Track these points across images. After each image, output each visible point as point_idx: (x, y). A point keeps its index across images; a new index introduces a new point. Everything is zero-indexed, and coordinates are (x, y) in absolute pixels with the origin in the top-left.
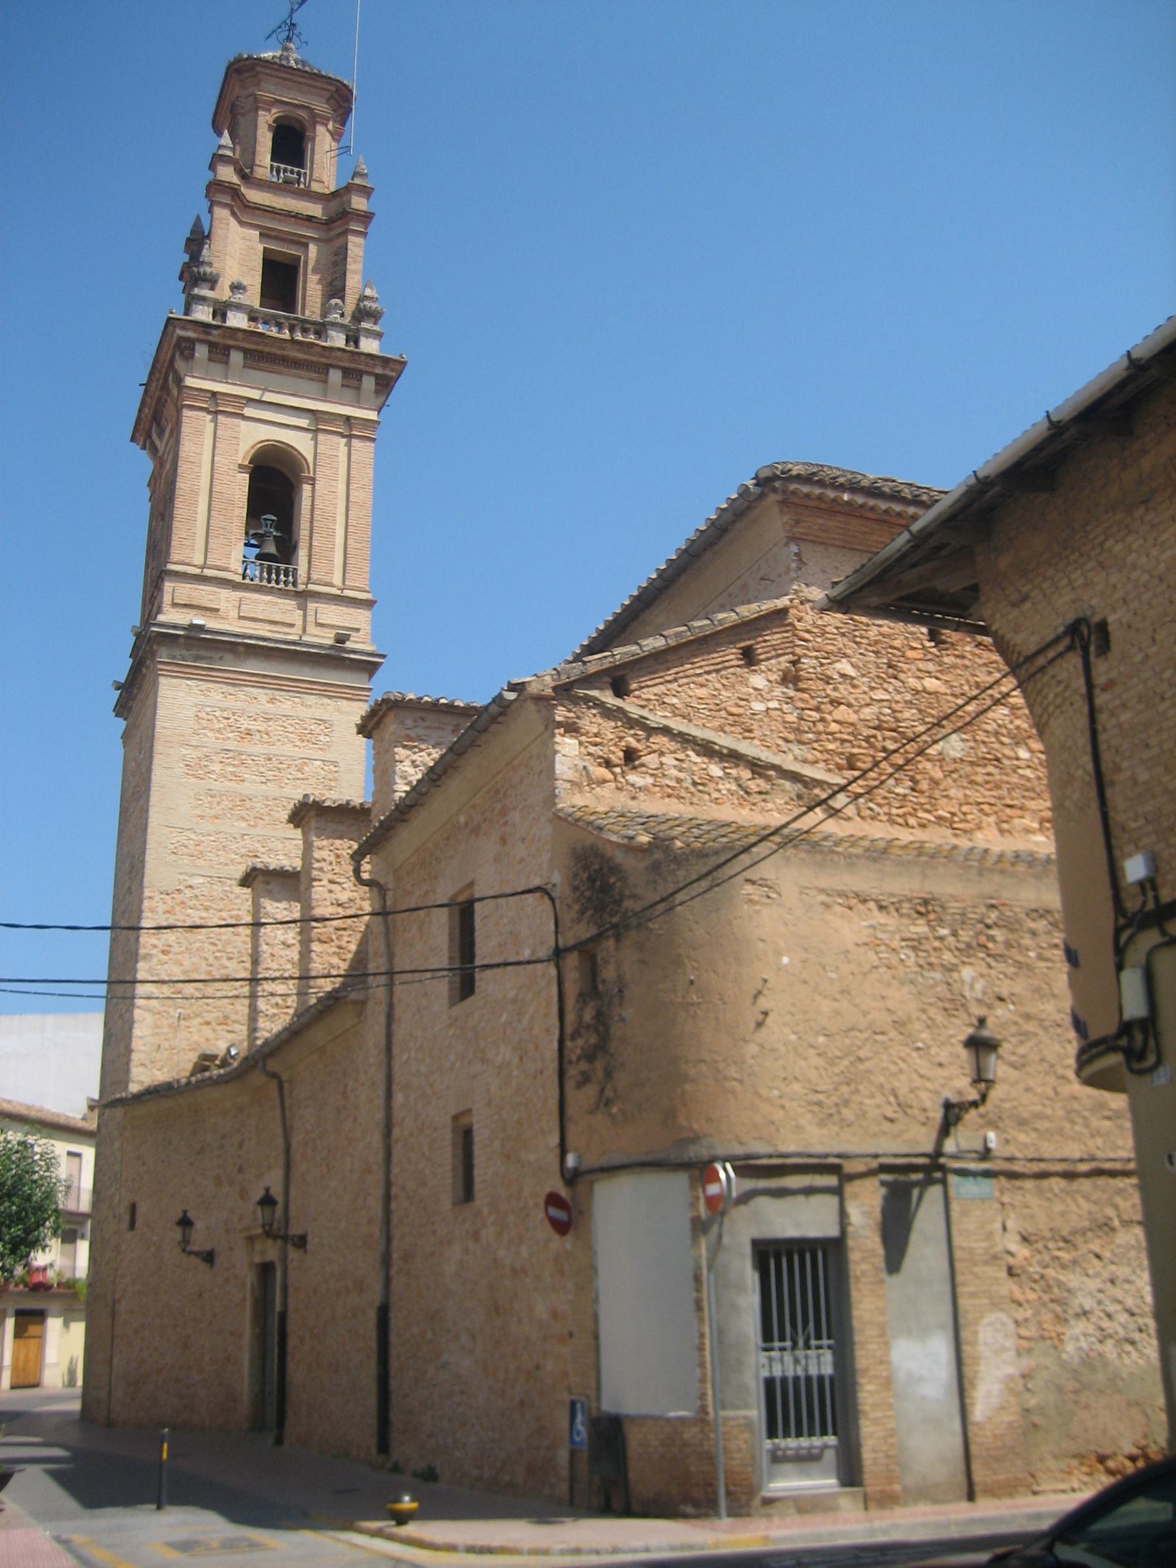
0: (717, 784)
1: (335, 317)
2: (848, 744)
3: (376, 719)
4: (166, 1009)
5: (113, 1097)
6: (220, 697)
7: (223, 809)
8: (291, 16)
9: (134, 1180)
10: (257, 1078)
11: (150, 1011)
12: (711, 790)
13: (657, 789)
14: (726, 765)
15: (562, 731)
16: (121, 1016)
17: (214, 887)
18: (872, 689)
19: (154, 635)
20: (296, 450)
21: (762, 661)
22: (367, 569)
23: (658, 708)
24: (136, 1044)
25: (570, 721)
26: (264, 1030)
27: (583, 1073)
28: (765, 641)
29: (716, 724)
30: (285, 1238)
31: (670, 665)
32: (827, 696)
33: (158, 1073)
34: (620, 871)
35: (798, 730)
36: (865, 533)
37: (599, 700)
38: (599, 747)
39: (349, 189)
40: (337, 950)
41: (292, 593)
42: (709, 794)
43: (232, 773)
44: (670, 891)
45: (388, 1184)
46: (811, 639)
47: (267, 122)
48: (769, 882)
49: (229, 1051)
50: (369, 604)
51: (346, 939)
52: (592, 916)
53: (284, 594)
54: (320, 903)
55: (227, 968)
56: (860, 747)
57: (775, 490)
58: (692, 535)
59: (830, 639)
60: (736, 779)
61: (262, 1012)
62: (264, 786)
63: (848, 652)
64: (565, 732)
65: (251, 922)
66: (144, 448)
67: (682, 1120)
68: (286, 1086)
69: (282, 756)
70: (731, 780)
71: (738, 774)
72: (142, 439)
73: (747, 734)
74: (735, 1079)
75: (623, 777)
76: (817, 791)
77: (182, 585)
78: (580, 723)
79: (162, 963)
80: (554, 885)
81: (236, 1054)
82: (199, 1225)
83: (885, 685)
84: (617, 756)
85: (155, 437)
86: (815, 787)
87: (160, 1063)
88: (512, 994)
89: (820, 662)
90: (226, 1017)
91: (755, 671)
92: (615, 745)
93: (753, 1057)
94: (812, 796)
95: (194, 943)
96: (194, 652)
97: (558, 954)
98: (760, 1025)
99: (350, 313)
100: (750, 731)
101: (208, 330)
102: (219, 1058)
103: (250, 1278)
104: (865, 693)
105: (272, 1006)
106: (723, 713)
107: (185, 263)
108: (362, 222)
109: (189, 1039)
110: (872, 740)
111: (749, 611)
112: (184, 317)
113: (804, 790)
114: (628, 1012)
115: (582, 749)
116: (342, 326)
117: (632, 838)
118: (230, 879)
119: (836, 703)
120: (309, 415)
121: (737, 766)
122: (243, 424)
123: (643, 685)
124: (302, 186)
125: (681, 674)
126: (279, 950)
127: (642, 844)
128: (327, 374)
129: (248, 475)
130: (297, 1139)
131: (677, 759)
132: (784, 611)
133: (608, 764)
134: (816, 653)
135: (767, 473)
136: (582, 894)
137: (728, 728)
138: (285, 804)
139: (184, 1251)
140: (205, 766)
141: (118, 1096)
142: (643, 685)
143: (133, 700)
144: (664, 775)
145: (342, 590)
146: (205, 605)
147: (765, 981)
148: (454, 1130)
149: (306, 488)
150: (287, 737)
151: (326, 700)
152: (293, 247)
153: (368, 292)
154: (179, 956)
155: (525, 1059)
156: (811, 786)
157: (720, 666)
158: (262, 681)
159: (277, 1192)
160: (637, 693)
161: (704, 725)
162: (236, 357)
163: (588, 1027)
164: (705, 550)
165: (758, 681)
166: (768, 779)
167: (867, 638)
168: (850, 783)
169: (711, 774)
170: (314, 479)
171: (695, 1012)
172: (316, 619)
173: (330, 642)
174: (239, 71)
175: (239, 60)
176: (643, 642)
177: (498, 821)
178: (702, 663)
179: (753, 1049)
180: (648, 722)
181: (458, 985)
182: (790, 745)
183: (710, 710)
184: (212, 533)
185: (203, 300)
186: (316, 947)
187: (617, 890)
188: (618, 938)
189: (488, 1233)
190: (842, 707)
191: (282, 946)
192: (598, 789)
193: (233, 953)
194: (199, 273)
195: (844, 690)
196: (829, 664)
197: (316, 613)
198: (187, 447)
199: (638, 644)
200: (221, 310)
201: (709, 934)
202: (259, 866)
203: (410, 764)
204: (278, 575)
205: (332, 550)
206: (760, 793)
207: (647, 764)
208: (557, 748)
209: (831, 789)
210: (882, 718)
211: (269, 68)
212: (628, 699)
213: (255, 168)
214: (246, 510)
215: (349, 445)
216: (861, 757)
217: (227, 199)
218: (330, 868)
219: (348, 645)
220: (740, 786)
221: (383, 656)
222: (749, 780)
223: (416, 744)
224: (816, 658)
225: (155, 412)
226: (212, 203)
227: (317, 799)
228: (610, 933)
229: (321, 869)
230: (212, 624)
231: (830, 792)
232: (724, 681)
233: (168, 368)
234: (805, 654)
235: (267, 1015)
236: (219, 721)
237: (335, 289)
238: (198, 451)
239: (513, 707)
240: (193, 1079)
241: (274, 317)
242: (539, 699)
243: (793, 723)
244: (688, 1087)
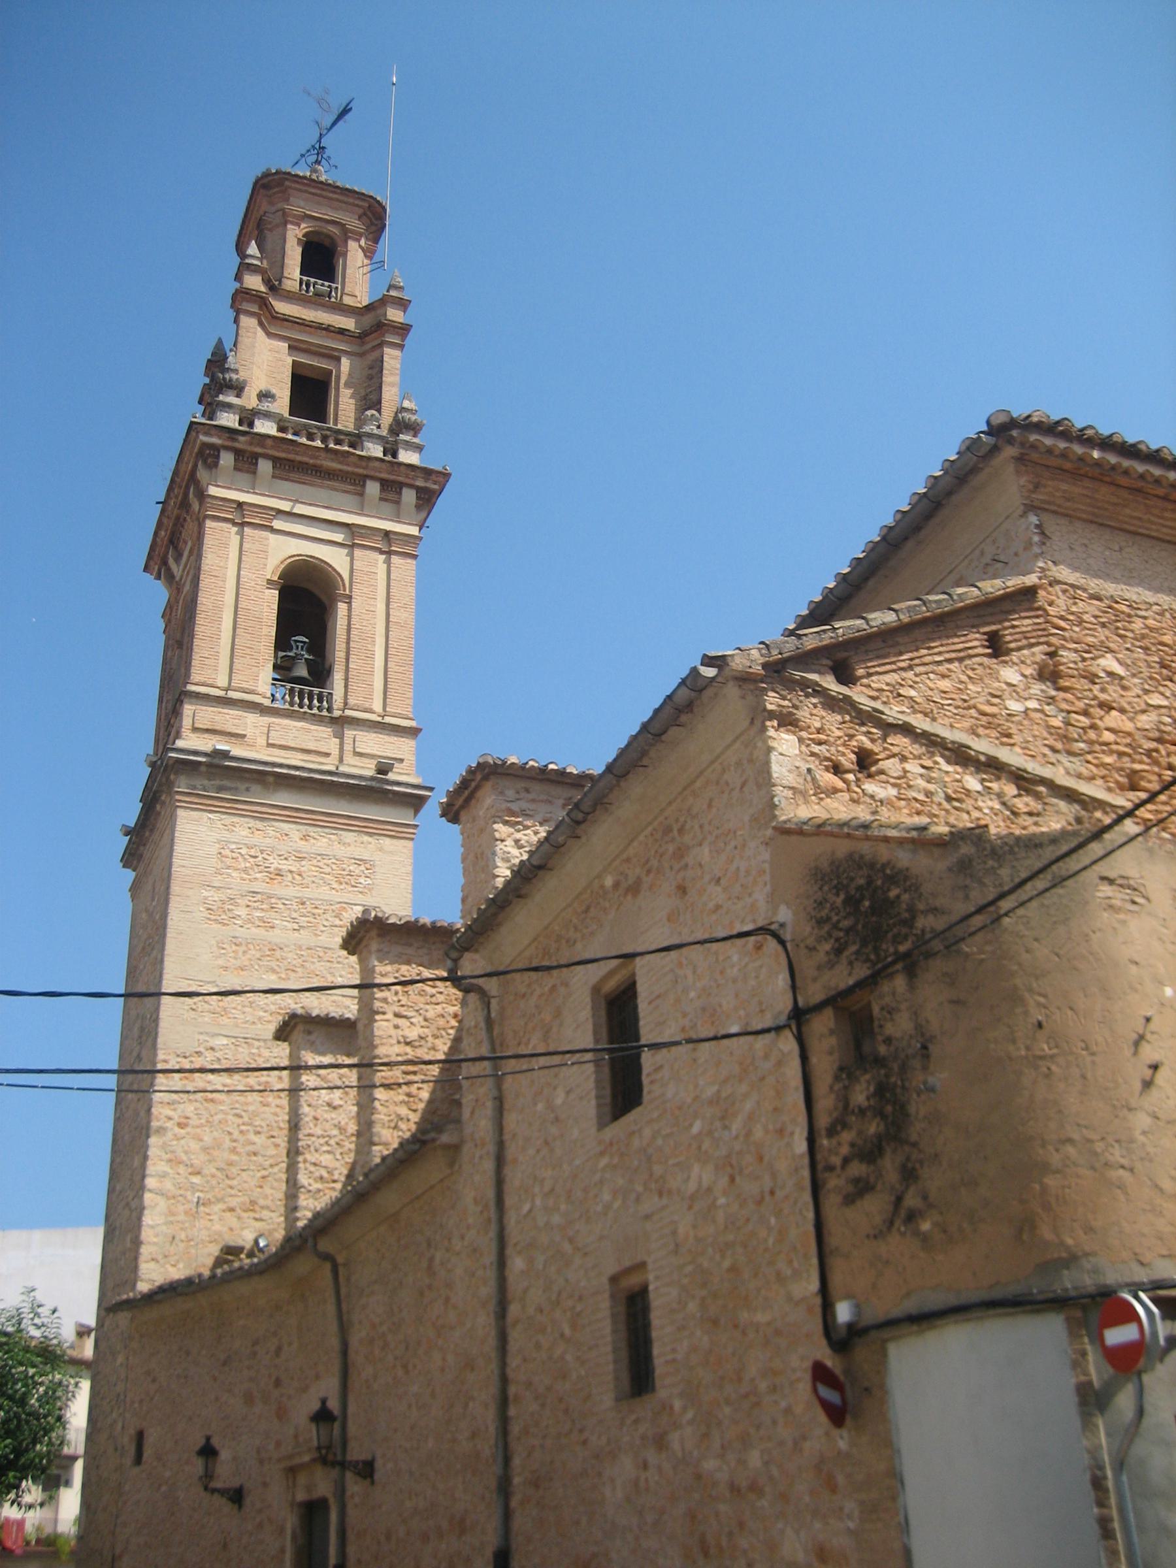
0: (976, 800)
1: (370, 428)
2: (1126, 759)
3: (467, 793)
4: (181, 1192)
5: (118, 1298)
6: (246, 832)
7: (250, 960)
8: (319, 141)
9: (141, 1401)
10: (303, 1265)
11: (163, 1194)
12: (970, 808)
13: (903, 803)
14: (985, 776)
15: (775, 723)
16: (128, 1204)
17: (240, 1049)
18: (1147, 692)
19: (171, 762)
20: (331, 566)
21: (1012, 650)
22: (411, 695)
23: (892, 701)
24: (146, 1234)
25: (785, 711)
26: (306, 1208)
27: (856, 1181)
28: (1014, 627)
29: (967, 724)
30: (343, 1465)
31: (902, 648)
32: (1095, 698)
33: (171, 1269)
34: (906, 878)
35: (1065, 738)
36: (1115, 504)
37: (820, 686)
39: (384, 301)
40: (406, 1099)
41: (327, 720)
42: (968, 813)
43: (261, 919)
44: (991, 897)
45: (504, 1380)
46: (1068, 627)
47: (296, 236)
48: (1132, 882)
49: (256, 1242)
50: (413, 732)
53: (318, 720)
54: (385, 1041)
55: (254, 1144)
56: (1141, 762)
57: (1011, 441)
58: (889, 521)
59: (1089, 629)
60: (1000, 796)
61: (303, 1187)
62: (296, 934)
63: (1111, 645)
64: (779, 725)
65: (358, 982)
66: (158, 577)
67: (1046, 1232)
68: (341, 1271)
69: (317, 899)
70: (993, 797)
71: (1001, 788)
72: (156, 567)
73: (1005, 740)
74: (1123, 1167)
75: (859, 787)
76: (1098, 814)
77: (204, 708)
78: (799, 714)
79: (178, 1138)
80: (782, 925)
81: (267, 1246)
82: (224, 1455)
83: (1161, 689)
84: (848, 760)
85: (171, 561)
86: (1095, 809)
87: (176, 1257)
88: (710, 1091)
89: (1081, 656)
90: (253, 1203)
91: (1006, 662)
92: (844, 745)
93: (1144, 1133)
94: (1093, 821)
95: (216, 1114)
96: (218, 782)
97: (799, 1016)
98: (1148, 1084)
99: (387, 426)
100: (1009, 736)
101: (236, 437)
102: (245, 1251)
103: (291, 1521)
104: (1139, 696)
105: (315, 1180)
106: (973, 711)
107: (205, 384)
108: (398, 334)
109: (208, 1229)
110: (1154, 754)
111: (992, 587)
112: (208, 422)
113: (1083, 813)
114: (939, 1077)
115: (803, 748)
116: (380, 437)
117: (924, 828)
118: (258, 1040)
119: (1107, 707)
120: (344, 530)
121: (998, 778)
122: (272, 537)
123: (872, 670)
124: (333, 300)
125: (917, 661)
126: (325, 1114)
127: (941, 835)
128: (364, 486)
129: (277, 592)
130: (356, 1338)
131: (923, 767)
132: (1030, 592)
133: (837, 769)
134: (1075, 645)
135: (1002, 419)
136: (836, 926)
137: (981, 731)
138: (321, 954)
139: (206, 1489)
140: (229, 910)
141: (125, 1297)
142: (872, 670)
143: (144, 845)
144: (910, 786)
145: (383, 717)
146: (229, 730)
147: (1148, 1020)
148: (613, 1296)
149: (342, 607)
150: (323, 879)
151: (366, 838)
152: (325, 361)
153: (406, 404)
154: (198, 1130)
155: (738, 1179)
156: (1090, 807)
157: (962, 654)
158: (294, 816)
159: (334, 1405)
160: (865, 681)
161: (952, 726)
162: (265, 466)
163: (862, 1112)
164: (906, 539)
165: (1010, 674)
166: (1037, 796)
167: (1132, 631)
168: (1137, 806)
170: (350, 597)
171: (1049, 1069)
172: (354, 748)
173: (370, 773)
174: (266, 187)
175: (267, 174)
176: (871, 616)
177: (671, 868)
178: (940, 649)
179: (1141, 1121)
180: (884, 717)
181: (608, 1100)
182: (1058, 756)
183: (957, 707)
184: (237, 652)
185: (228, 407)
186: (380, 1094)
187: (904, 906)
188: (911, 972)
189: (682, 1439)
190: (1114, 713)
191: (327, 1108)
192: (829, 800)
193: (262, 1127)
194: (224, 379)
195: (1113, 693)
196: (1092, 659)
197: (354, 741)
198: (210, 560)
199: (863, 618)
200: (248, 417)
201: (1057, 955)
202: (300, 1011)
203: (513, 843)
204: (311, 699)
205: (372, 673)
206: (1030, 814)
207: (888, 772)
208: (771, 743)
209: (1116, 813)
210: (1163, 727)
211: (298, 182)
212: (858, 688)
213: (284, 280)
214: (275, 629)
215: (388, 563)
216: (1144, 774)
217: (254, 308)
218: (395, 999)
219: (391, 776)
220: (1004, 804)
221: (431, 789)
222: (1015, 797)
223: (520, 819)
224: (1076, 651)
225: (173, 533)
226: (238, 312)
227: (380, 915)
228: (899, 966)
229: (385, 1000)
230: (236, 751)
231: (1114, 816)
232: (970, 673)
233: (188, 481)
234: (1062, 645)
235: (309, 1191)
236: (245, 859)
237: (370, 400)
238: (222, 564)
240: (219, 1271)
241: (305, 426)
242: (745, 679)
243: (1060, 728)
244: (1051, 1181)
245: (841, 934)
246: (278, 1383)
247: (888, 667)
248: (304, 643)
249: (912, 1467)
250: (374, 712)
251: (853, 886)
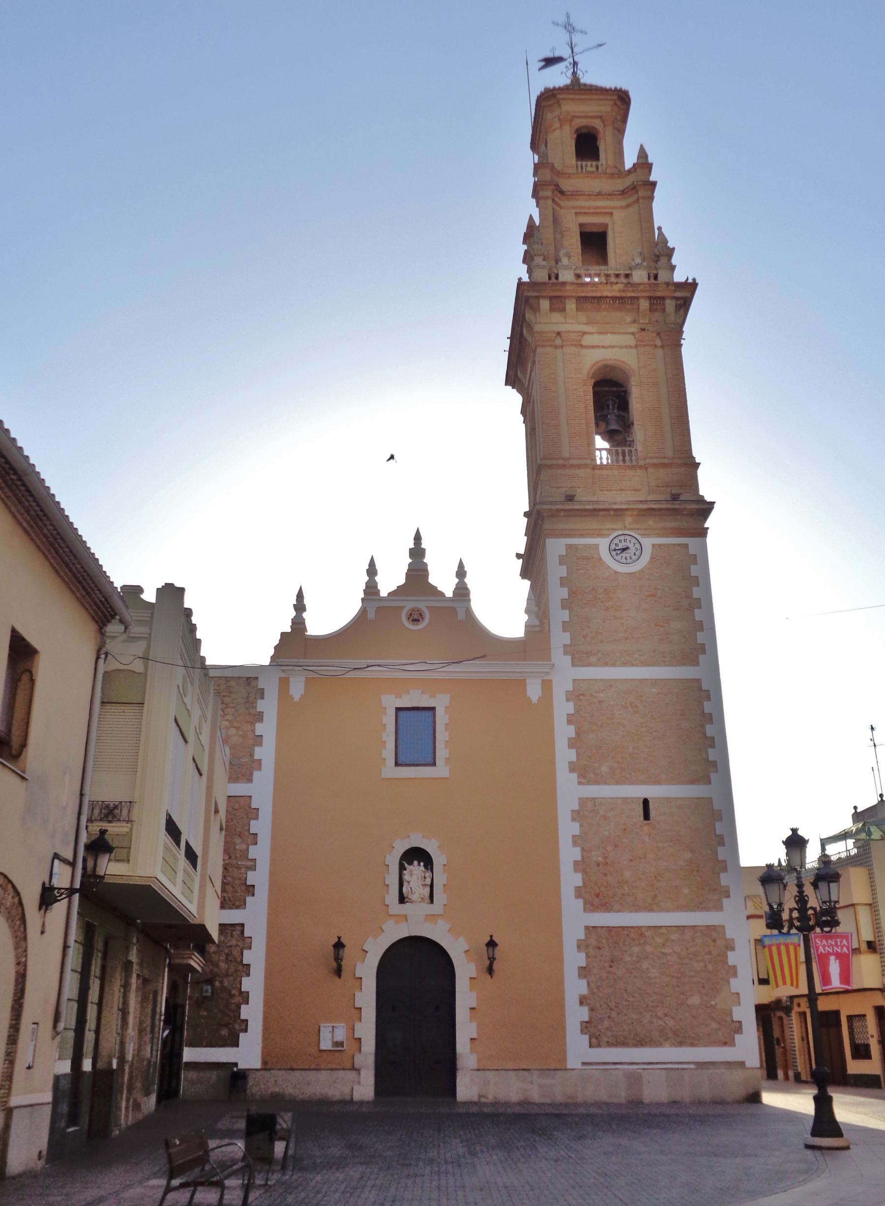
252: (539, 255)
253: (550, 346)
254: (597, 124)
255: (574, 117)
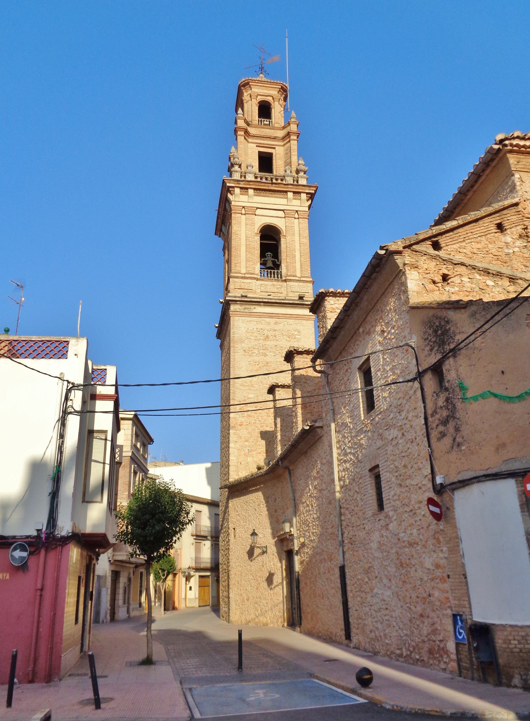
28: (508, 220)
38: (429, 275)
51: (312, 407)
52: (437, 350)
66: (220, 236)
75: (443, 288)
82: (260, 535)
84: (438, 278)
125: (467, 238)
131: (469, 278)
165: (509, 239)
169: (488, 284)
188: (455, 356)
228: (450, 354)
239: (385, 259)
245: (432, 343)
246: (276, 511)
247: (455, 242)
248: (271, 255)
249: (463, 533)
250: (297, 277)
251: (435, 325)
252: (236, 164)
253: (239, 213)
254: (270, 99)
255: (258, 95)
